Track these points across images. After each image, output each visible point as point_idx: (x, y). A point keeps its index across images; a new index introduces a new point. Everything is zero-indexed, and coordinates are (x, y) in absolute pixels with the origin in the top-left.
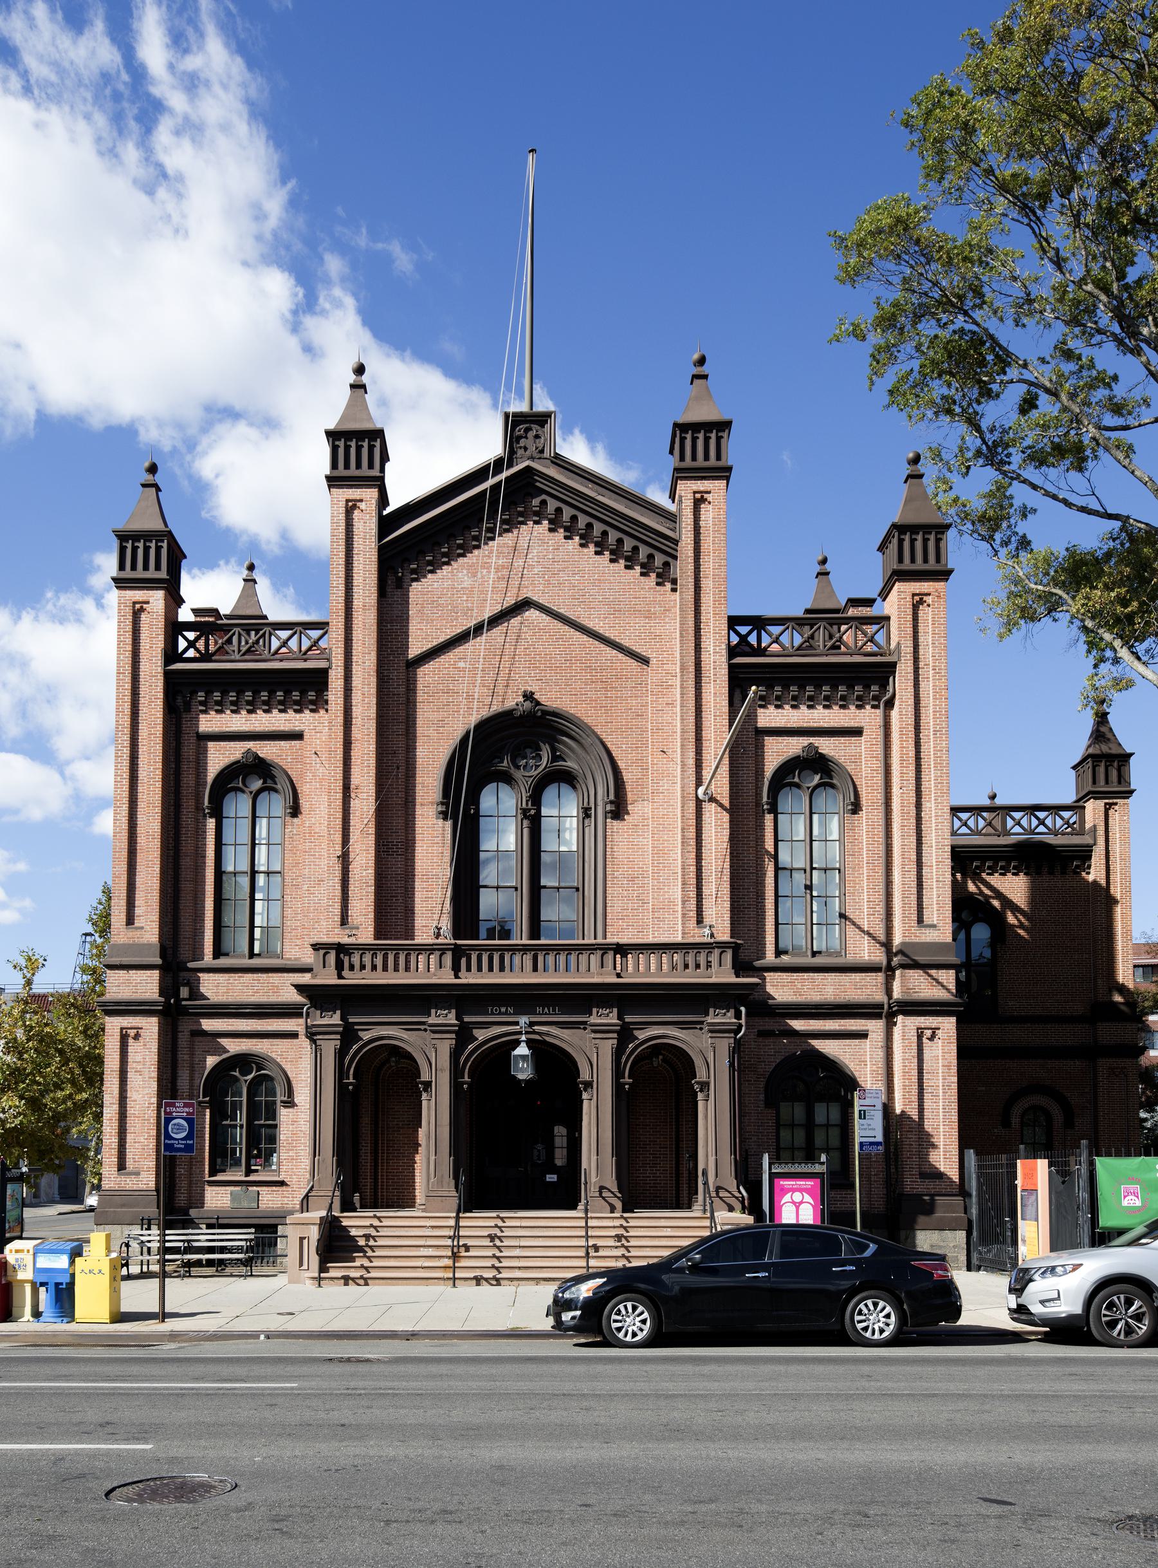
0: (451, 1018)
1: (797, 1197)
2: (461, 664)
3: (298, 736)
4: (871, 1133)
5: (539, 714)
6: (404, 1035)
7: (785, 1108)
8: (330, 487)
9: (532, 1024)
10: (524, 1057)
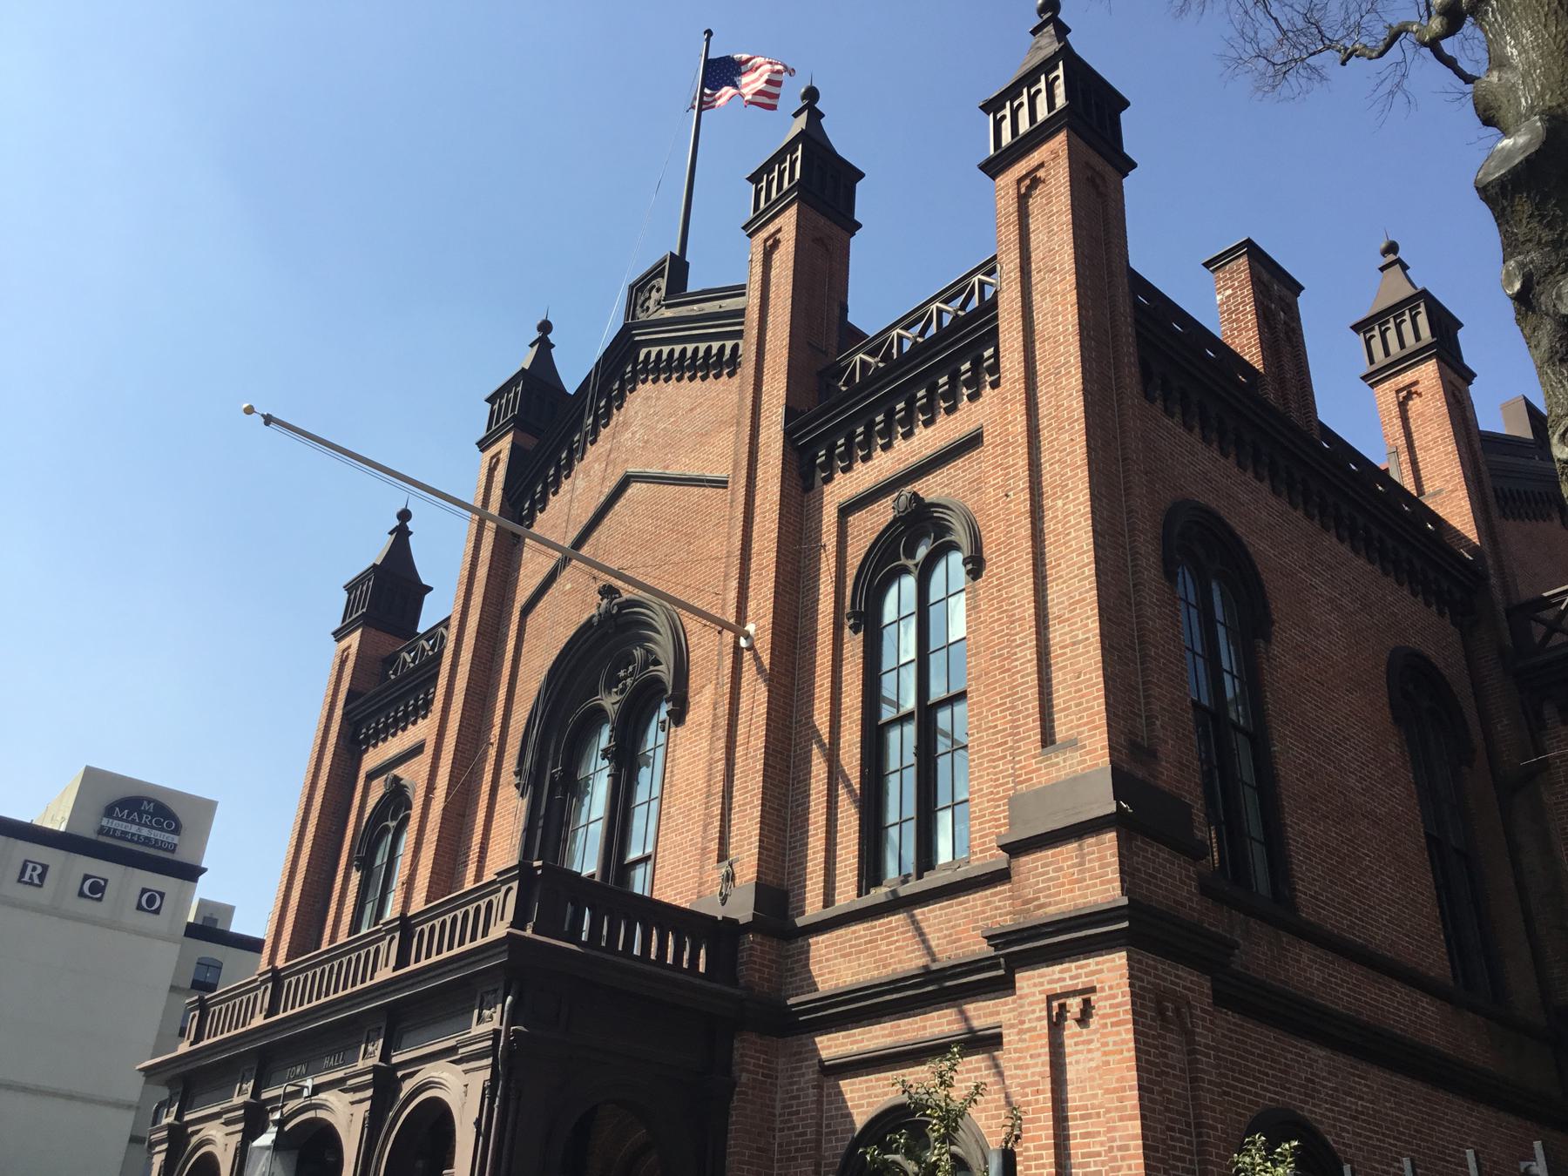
3: (972, 442)
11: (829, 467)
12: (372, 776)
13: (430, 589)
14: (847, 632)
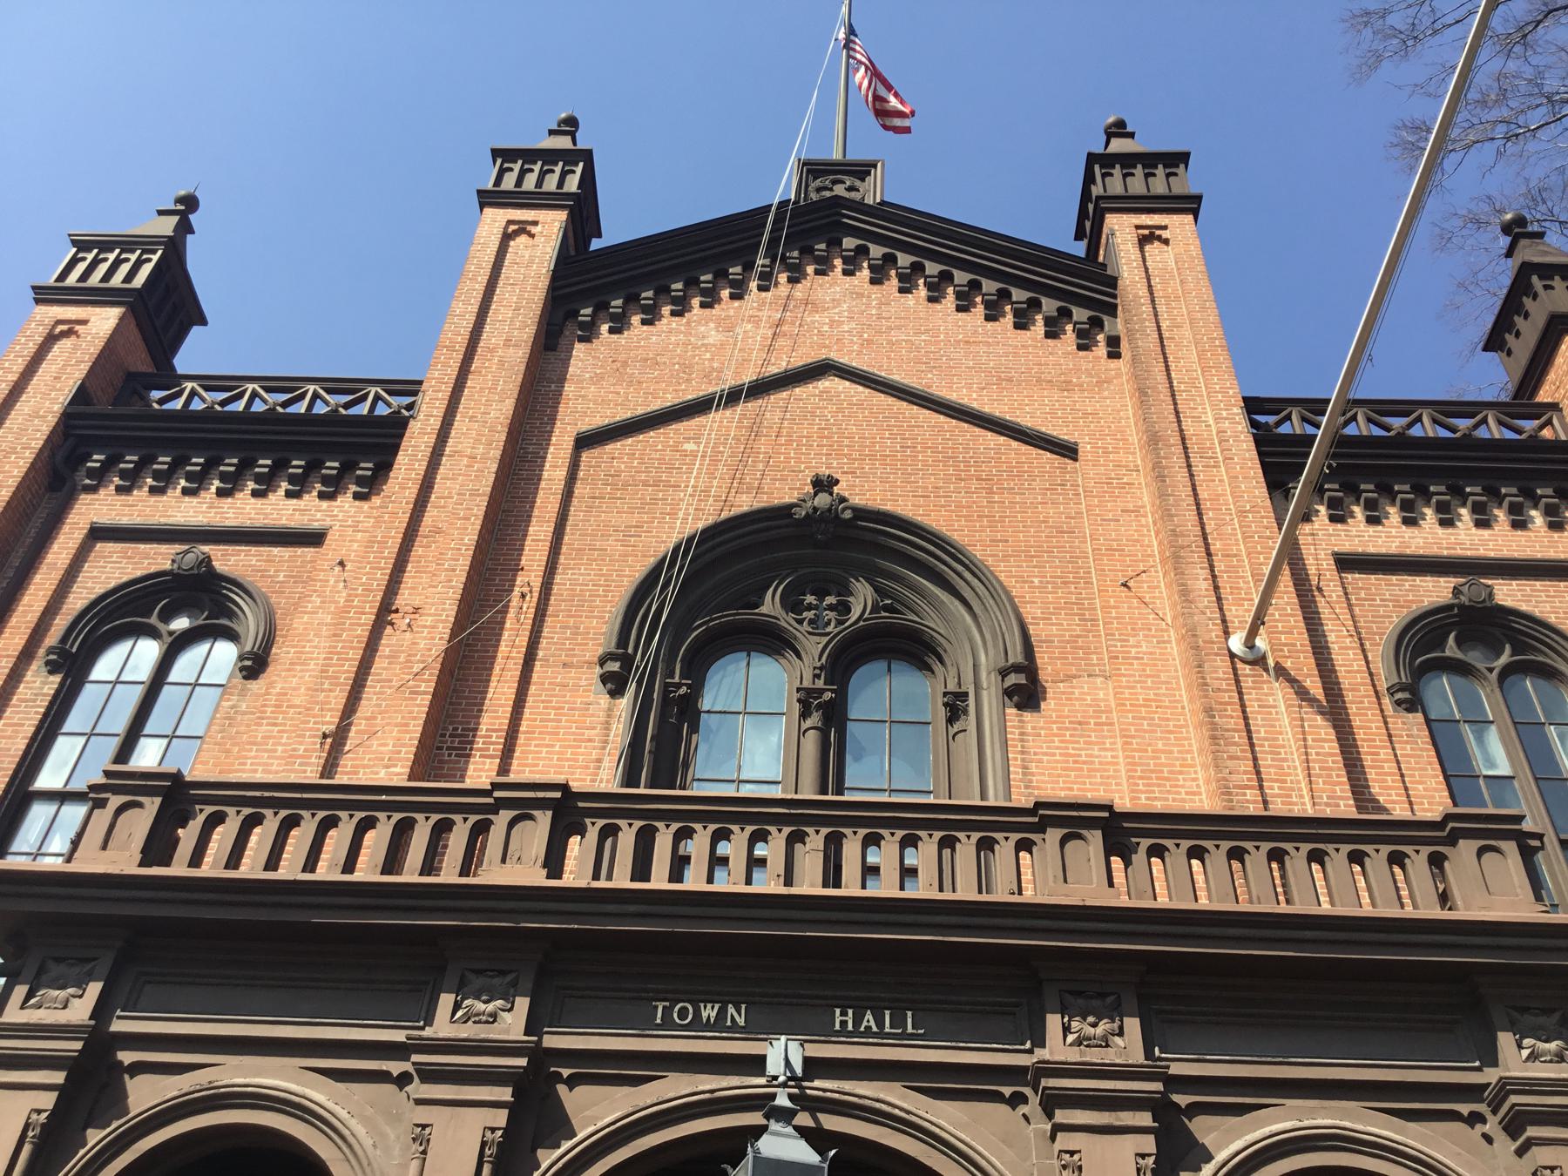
0: (512, 1023)
2: (690, 446)
3: (313, 538)
5: (848, 515)
6: (320, 1093)
8: (482, 206)
9: (814, 1067)
11: (100, 477)
13: (204, 322)
14: (37, 665)
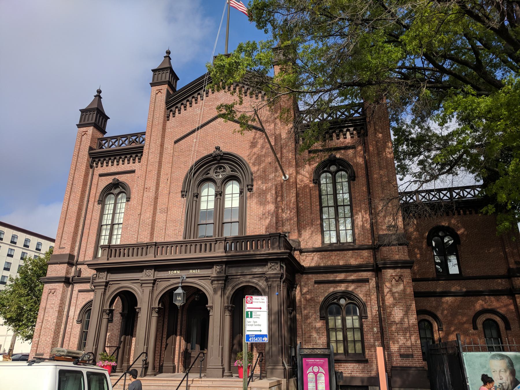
1: (316, 369)
3: (133, 172)
4: (258, 328)
7: (331, 319)
10: (179, 294)
12: (101, 175)
13: (109, 118)
